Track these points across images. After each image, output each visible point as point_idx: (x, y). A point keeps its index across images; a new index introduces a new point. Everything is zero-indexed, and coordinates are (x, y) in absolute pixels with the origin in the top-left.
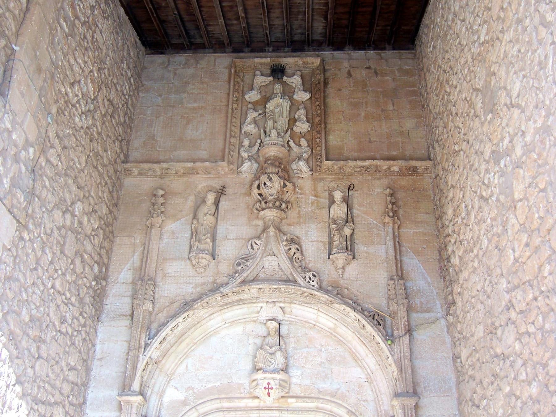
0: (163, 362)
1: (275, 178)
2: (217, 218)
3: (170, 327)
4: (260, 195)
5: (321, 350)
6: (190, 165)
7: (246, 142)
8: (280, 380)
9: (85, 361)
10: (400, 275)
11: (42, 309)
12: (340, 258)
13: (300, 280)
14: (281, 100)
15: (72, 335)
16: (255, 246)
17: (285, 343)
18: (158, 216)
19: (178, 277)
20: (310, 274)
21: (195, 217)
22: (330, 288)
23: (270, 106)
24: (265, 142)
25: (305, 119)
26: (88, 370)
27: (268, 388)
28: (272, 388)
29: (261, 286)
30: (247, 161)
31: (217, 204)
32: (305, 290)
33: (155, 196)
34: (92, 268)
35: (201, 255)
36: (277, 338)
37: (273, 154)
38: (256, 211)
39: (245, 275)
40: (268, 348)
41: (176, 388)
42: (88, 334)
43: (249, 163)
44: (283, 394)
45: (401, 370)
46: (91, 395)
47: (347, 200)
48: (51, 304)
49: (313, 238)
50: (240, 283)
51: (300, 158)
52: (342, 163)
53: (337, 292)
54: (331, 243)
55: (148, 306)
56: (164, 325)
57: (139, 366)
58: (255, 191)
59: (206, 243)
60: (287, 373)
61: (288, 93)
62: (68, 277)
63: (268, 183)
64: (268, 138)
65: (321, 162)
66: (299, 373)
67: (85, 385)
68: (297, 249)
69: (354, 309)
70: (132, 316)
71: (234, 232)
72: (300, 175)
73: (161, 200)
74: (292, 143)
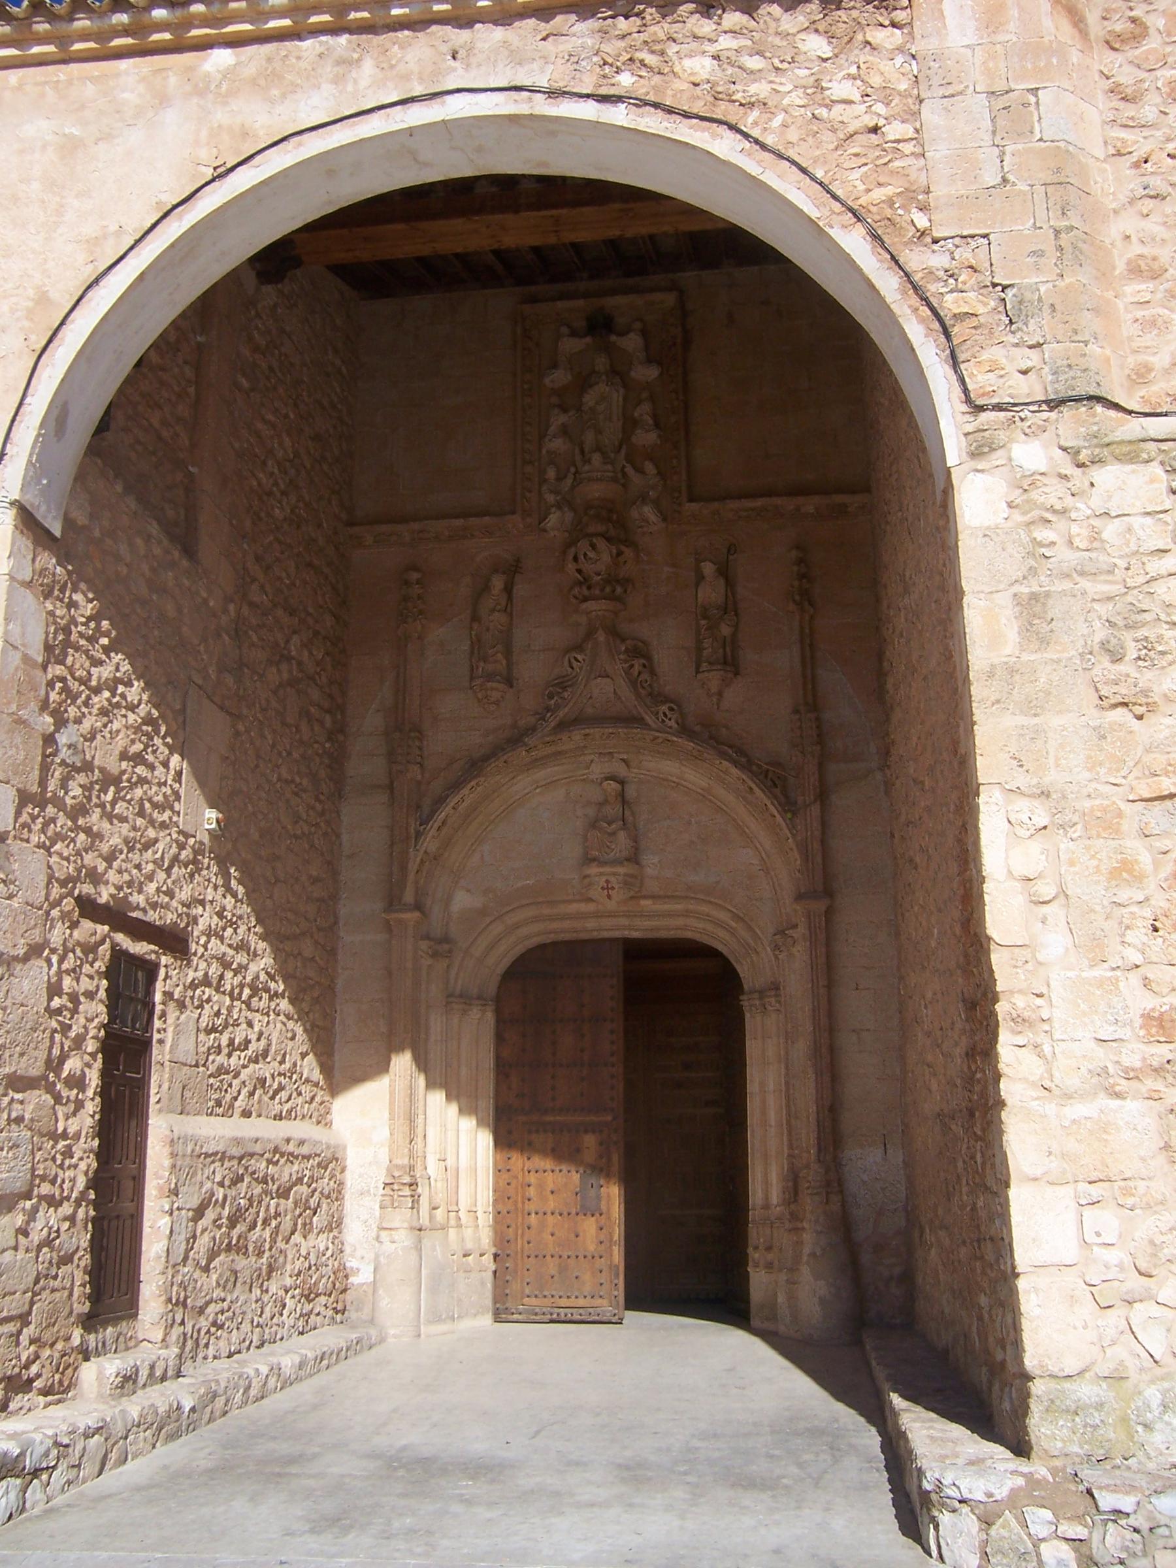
0: (446, 855)
1: (601, 543)
2: (511, 615)
3: (452, 804)
4: (579, 571)
5: (689, 823)
6: (459, 522)
7: (551, 473)
8: (625, 875)
9: (329, 863)
10: (811, 702)
11: (271, 816)
12: (714, 679)
13: (649, 719)
14: (607, 389)
15: (310, 833)
16: (575, 664)
17: (633, 814)
18: (415, 620)
19: (459, 720)
20: (664, 708)
21: (475, 618)
22: (698, 728)
23: (589, 399)
24: (584, 475)
25: (651, 422)
26: (335, 873)
27: (608, 888)
28: (613, 888)
29: (587, 731)
30: (553, 510)
31: (508, 589)
32: (657, 734)
33: (407, 583)
34: (321, 723)
35: (490, 684)
36: (619, 808)
37: (597, 495)
38: (574, 601)
39: (561, 714)
40: (605, 825)
41: (468, 891)
42: (328, 823)
43: (558, 514)
44: (632, 893)
45: (806, 857)
46: (343, 912)
47: (725, 572)
48: (280, 804)
49: (669, 642)
50: (554, 728)
51: (644, 498)
52: (716, 505)
53: (708, 736)
54: (699, 649)
55: (414, 772)
56: (440, 801)
57: (410, 866)
58: (571, 567)
59: (496, 661)
60: (637, 863)
61: (618, 374)
62: (295, 755)
63: (591, 554)
64: (587, 468)
65: (680, 504)
66: (656, 860)
67: (334, 897)
68: (644, 666)
69: (736, 763)
70: (391, 787)
71: (539, 638)
72: (645, 529)
73: (416, 590)
74: (629, 470)
